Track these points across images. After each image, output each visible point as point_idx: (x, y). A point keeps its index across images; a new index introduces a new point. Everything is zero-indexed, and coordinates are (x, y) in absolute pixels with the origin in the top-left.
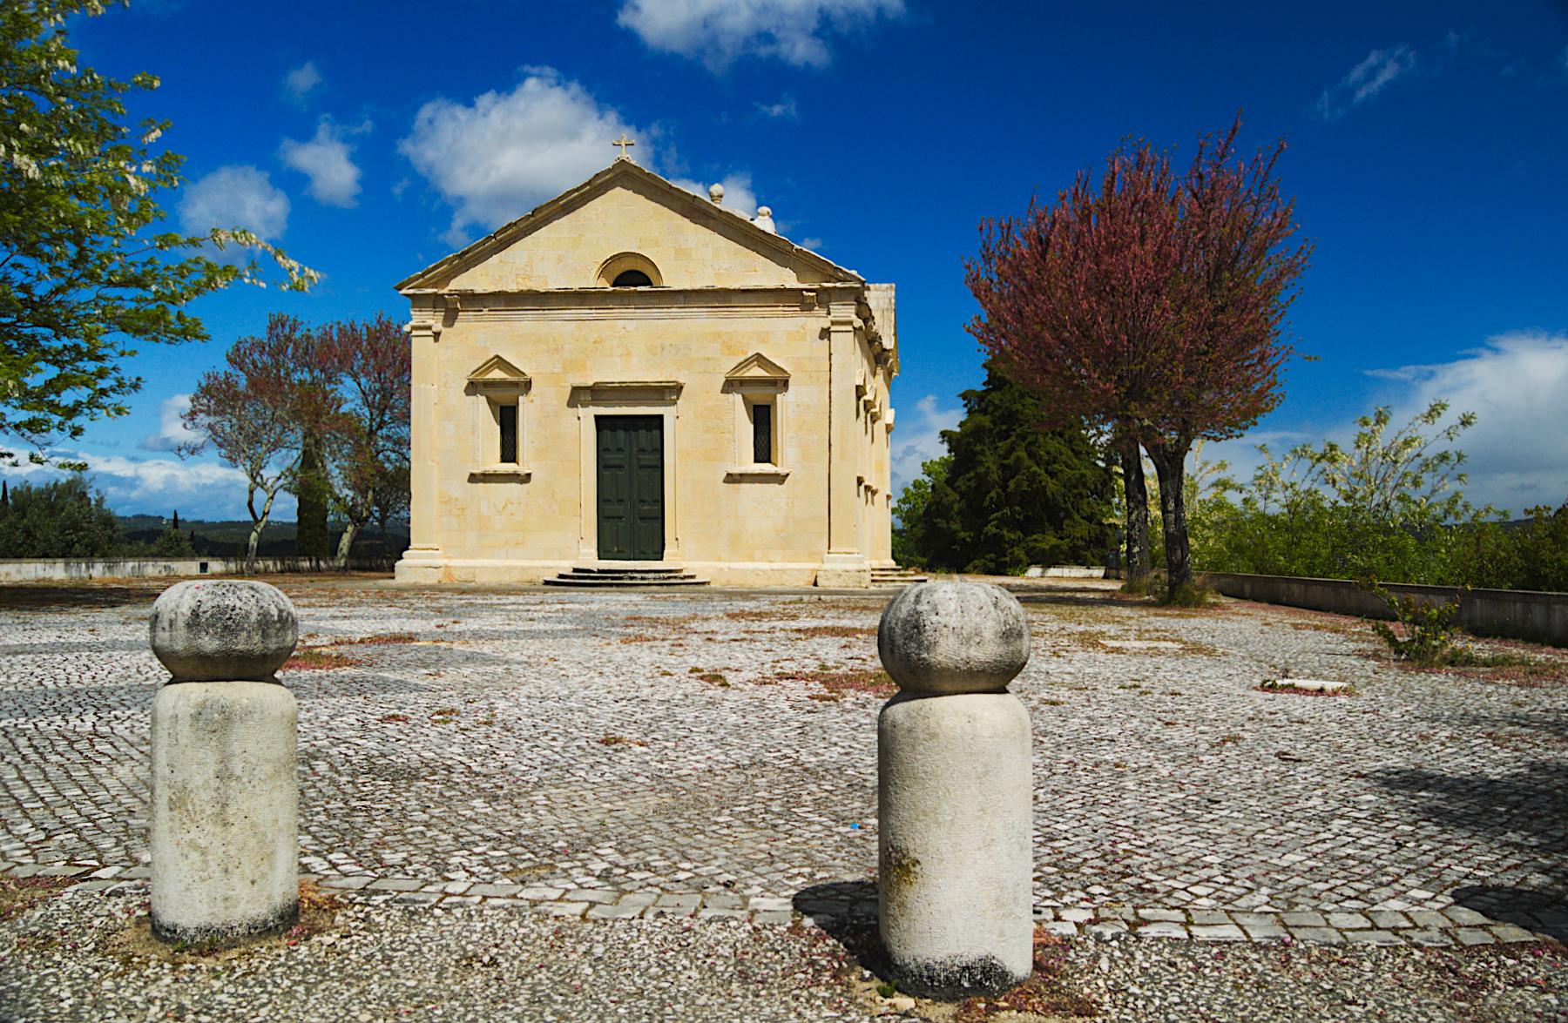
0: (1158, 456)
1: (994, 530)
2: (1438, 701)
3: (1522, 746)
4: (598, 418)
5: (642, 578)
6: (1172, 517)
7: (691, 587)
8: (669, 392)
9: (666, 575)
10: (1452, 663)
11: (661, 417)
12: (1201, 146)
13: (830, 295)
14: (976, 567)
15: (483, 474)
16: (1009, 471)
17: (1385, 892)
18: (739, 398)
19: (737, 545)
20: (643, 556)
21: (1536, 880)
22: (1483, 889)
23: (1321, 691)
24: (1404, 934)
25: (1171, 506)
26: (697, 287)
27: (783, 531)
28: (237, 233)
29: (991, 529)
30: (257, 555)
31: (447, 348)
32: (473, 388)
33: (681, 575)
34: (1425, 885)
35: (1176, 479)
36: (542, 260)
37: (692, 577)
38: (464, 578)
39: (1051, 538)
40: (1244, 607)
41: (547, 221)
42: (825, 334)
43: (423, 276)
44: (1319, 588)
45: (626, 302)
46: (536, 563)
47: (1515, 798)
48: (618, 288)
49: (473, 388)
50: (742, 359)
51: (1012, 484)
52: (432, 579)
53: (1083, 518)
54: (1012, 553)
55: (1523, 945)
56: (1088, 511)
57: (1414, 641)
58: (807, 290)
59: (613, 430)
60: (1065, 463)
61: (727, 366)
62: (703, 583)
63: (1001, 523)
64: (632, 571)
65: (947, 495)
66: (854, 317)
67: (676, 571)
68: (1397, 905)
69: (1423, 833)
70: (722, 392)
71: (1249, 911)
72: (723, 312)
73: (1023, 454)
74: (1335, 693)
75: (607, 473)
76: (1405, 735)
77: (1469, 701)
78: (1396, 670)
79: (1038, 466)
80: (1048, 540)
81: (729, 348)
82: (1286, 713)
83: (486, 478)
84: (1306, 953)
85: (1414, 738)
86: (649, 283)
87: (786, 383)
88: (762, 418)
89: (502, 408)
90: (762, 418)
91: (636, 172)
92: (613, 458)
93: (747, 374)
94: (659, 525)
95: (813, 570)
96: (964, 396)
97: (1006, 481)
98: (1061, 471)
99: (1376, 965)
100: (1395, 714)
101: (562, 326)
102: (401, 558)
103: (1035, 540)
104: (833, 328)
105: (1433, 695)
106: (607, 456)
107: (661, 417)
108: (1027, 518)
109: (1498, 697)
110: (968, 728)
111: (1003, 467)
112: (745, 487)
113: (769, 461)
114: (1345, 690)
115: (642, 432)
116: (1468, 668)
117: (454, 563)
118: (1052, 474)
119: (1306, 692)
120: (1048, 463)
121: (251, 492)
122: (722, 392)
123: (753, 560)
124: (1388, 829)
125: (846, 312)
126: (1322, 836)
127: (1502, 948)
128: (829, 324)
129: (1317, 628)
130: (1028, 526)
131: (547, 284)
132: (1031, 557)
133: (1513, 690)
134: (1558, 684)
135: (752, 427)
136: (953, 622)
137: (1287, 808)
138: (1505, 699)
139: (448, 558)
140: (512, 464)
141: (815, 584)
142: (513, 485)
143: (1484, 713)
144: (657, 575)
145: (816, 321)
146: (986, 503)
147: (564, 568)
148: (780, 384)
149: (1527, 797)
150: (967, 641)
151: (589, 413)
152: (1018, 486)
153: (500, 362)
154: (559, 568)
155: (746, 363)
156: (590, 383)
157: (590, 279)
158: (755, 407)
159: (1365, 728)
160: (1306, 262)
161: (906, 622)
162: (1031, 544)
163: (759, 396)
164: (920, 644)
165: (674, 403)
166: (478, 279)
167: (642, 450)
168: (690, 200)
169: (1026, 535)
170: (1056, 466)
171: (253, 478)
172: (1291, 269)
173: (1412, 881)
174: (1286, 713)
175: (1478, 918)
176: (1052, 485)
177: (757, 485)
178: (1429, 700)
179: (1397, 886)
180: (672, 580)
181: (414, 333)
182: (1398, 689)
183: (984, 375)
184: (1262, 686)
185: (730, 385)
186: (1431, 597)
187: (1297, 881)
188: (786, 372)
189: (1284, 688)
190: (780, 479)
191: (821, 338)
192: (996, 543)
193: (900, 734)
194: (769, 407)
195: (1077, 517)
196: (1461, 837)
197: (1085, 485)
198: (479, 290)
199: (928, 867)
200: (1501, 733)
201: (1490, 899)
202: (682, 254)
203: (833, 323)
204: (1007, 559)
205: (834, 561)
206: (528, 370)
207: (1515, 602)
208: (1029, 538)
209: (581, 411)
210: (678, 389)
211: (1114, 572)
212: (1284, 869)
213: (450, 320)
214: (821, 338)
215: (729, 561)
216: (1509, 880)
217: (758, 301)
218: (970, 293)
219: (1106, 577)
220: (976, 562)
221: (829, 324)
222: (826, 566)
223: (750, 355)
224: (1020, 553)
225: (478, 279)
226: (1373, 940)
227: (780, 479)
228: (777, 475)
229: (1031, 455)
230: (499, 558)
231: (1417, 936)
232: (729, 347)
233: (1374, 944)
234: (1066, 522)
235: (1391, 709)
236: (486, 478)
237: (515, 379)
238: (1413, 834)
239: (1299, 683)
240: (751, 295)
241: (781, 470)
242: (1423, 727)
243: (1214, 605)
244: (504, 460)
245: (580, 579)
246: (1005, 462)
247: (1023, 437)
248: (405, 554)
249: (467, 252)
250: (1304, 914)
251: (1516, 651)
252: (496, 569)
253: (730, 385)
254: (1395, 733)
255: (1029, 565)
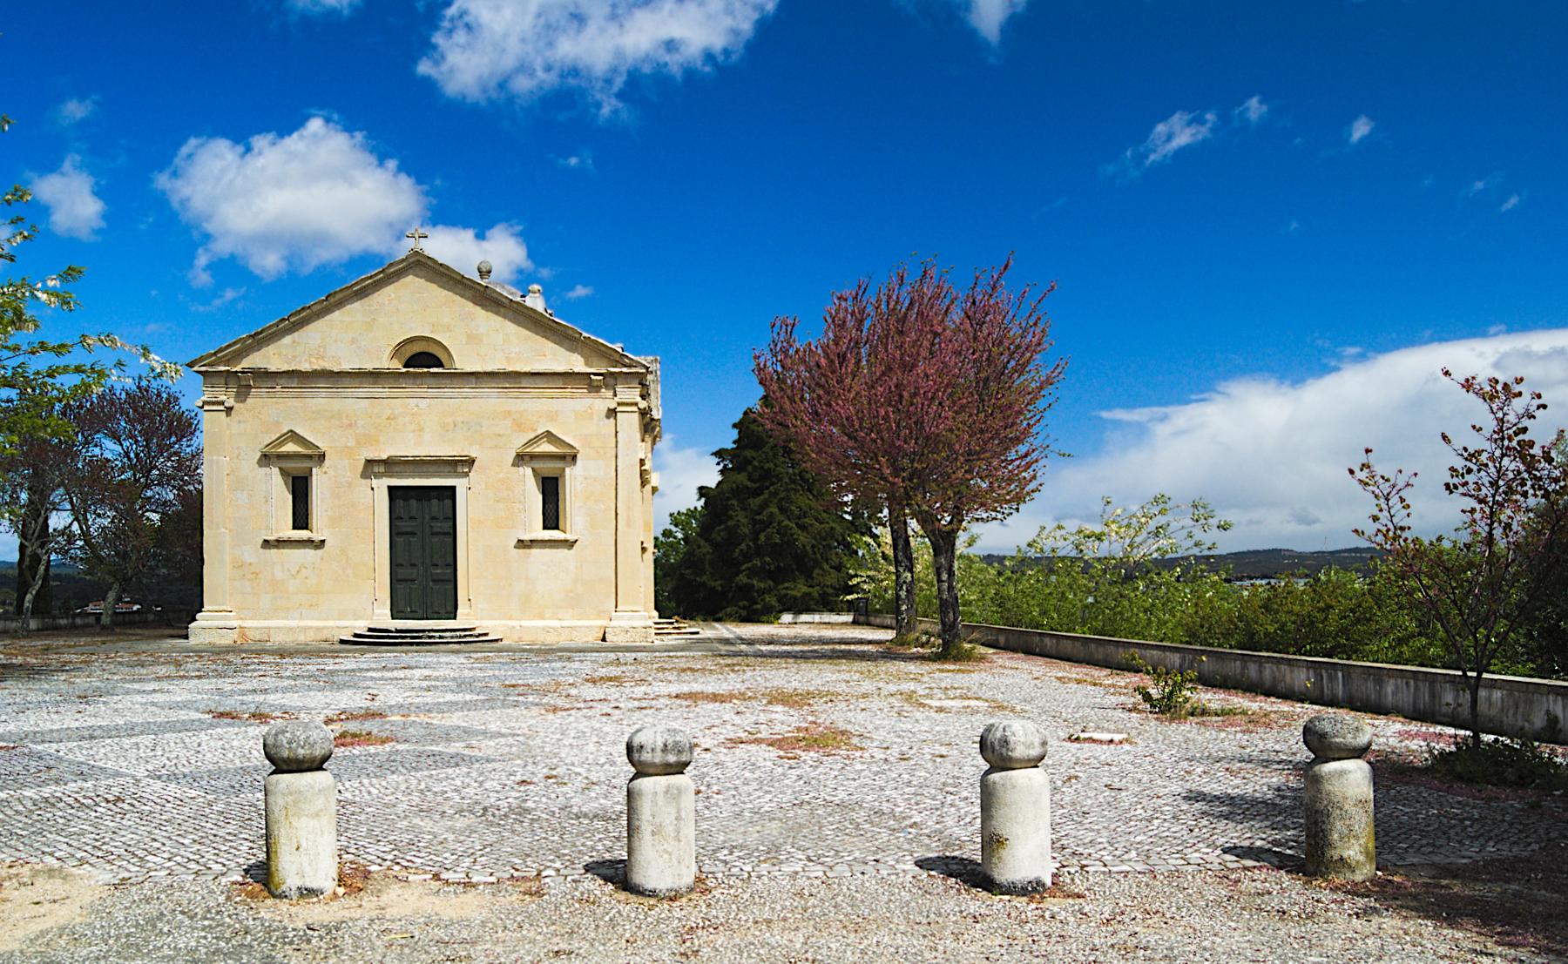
0: (934, 535)
1: (745, 580)
2: (1190, 746)
3: (1247, 776)
4: (391, 489)
5: (441, 637)
6: (945, 585)
7: (486, 645)
8: (461, 465)
9: (463, 634)
10: (1192, 714)
11: (453, 489)
12: (977, 278)
13: (616, 379)
14: (731, 616)
15: (278, 541)
16: (759, 526)
17: (1190, 850)
18: (529, 471)
20: (435, 616)
21: (1259, 843)
22: (1235, 847)
23: (1111, 741)
24: (1202, 866)
25: (945, 576)
26: (489, 369)
27: (572, 591)
28: (102, 338)
29: (742, 579)
30: (32, 614)
31: (240, 422)
32: (266, 459)
33: (476, 632)
34: (1208, 846)
35: (949, 554)
36: (336, 341)
37: (486, 635)
38: (258, 638)
39: (801, 586)
40: (1003, 659)
41: (340, 304)
42: (612, 413)
43: (215, 354)
44: (1069, 642)
45: (419, 381)
46: (331, 623)
47: (1246, 806)
48: (411, 370)
49: (266, 459)
51: (762, 537)
52: (227, 639)
53: (831, 567)
54: (763, 600)
55: (1254, 867)
56: (837, 561)
57: (1164, 698)
58: (595, 374)
59: (406, 499)
60: (814, 517)
61: (517, 443)
62: (497, 640)
63: (753, 572)
64: (429, 631)
65: (699, 547)
66: (639, 399)
67: (470, 630)
68: (1197, 855)
69: (1201, 825)
70: (513, 465)
71: (1130, 860)
72: (514, 393)
73: (775, 510)
74: (1121, 742)
75: (400, 539)
76: (1176, 771)
77: (1211, 746)
78: (1154, 722)
79: (789, 519)
80: (800, 589)
81: (519, 426)
82: (1095, 758)
83: (280, 543)
84: (1162, 874)
85: (1182, 773)
86: (441, 365)
87: (574, 457)
88: (551, 489)
89: (294, 478)
90: (551, 489)
91: (430, 263)
92: (406, 526)
93: (537, 450)
94: (452, 586)
95: (601, 627)
96: (715, 454)
97: (756, 535)
98: (812, 525)
99: (1193, 877)
100: (1164, 757)
101: (355, 404)
102: (194, 619)
103: (787, 588)
104: (619, 409)
105: (1185, 742)
106: (398, 523)
107: (453, 489)
108: (778, 568)
109: (1229, 740)
111: (755, 522)
112: (535, 552)
113: (557, 528)
114: (1127, 740)
115: (435, 502)
116: (1204, 719)
117: (247, 624)
118: (802, 527)
119: (1101, 742)
120: (799, 518)
122: (513, 465)
124: (1183, 824)
125: (631, 394)
126: (1151, 828)
127: (1246, 868)
128: (615, 405)
129: (1079, 682)
130: (778, 576)
131: (340, 364)
132: (783, 604)
133: (1239, 735)
134: (1268, 730)
135: (540, 497)
136: (1022, 739)
137: (1128, 816)
138: (1235, 743)
139: (241, 619)
140: (305, 531)
141: (604, 639)
142: (307, 550)
143: (1222, 755)
144: (453, 634)
145: (604, 401)
146: (736, 555)
147: (359, 628)
148: (569, 459)
149: (1252, 805)
150: (1028, 747)
151: (382, 485)
152: (768, 538)
153: (293, 436)
154: (354, 627)
155: (536, 439)
156: (384, 457)
157: (386, 362)
158: (544, 479)
159: (1150, 767)
160: (1061, 376)
161: (1000, 740)
162: (784, 592)
163: (548, 468)
164: (1008, 749)
165: (467, 475)
166: (271, 358)
167: (434, 518)
168: (482, 289)
169: (777, 583)
170: (807, 520)
172: (1048, 382)
173: (1201, 845)
174: (1095, 758)
175: (1235, 858)
176: (803, 539)
177: (547, 550)
178: (1184, 746)
179: (1195, 848)
180: (468, 639)
182: (1161, 738)
183: (735, 434)
184: (1069, 738)
185: (521, 459)
186: (1168, 654)
187: (1147, 847)
188: (575, 448)
189: (1085, 740)
190: (569, 544)
191: (608, 417)
192: (746, 590)
193: (998, 786)
194: (557, 479)
195: (826, 567)
196: (1222, 824)
197: (833, 537)
198: (273, 369)
199: (1012, 841)
200: (1234, 768)
201: (1238, 851)
203: (619, 404)
204: (759, 606)
205: (621, 618)
206: (323, 445)
207: (1235, 660)
208: (780, 587)
209: (375, 482)
210: (471, 462)
211: (862, 619)
212: (1139, 843)
213: (242, 395)
214: (608, 417)
216: (1246, 843)
217: (547, 383)
218: (757, 381)
219: (855, 623)
220: (729, 610)
221: (615, 405)
222: (613, 623)
223: (540, 432)
224: (771, 600)
225: (271, 358)
226: (1190, 868)
227: (569, 544)
228: (567, 541)
229: (782, 510)
230: (293, 618)
231: (1208, 866)
232: (519, 425)
233: (1190, 870)
234: (816, 571)
235: (1161, 753)
236: (280, 543)
237: (309, 452)
238: (1196, 825)
239: (1096, 736)
240: (538, 378)
241: (569, 536)
242: (1185, 764)
243: (982, 658)
244: (295, 527)
245: (375, 639)
246: (758, 517)
247: (775, 494)
248: (198, 616)
249: (261, 332)
250: (1154, 859)
251: (1239, 701)
252: (291, 629)
253: (521, 459)
254: (1170, 770)
255: (781, 612)
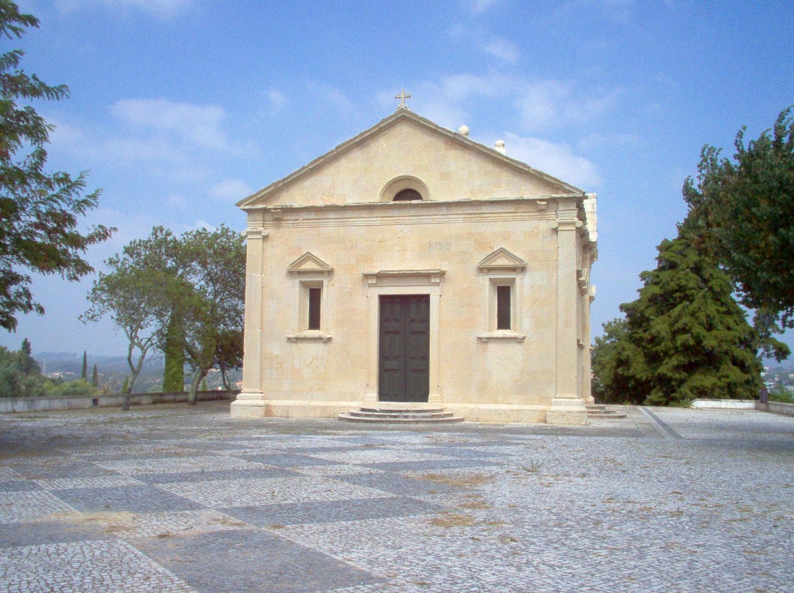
4: (490, 279)
11: (425, 299)
19: (484, 391)
32: (291, 273)
46: (333, 404)
49: (291, 273)
50: (490, 252)
61: (478, 258)
66: (576, 219)
83: (298, 340)
88: (504, 293)
93: (493, 264)
110: (608, 390)
121: (130, 350)
123: (496, 402)
145: (544, 226)
147: (354, 408)
153: (308, 257)
154: (350, 407)
156: (376, 271)
157: (375, 198)
171: (132, 339)
181: (249, 237)
185: (483, 270)
202: (445, 176)
215: (478, 403)
222: (553, 408)
223: (496, 249)
227: (520, 341)
236: (298, 340)
252: (304, 407)
253: (483, 270)
